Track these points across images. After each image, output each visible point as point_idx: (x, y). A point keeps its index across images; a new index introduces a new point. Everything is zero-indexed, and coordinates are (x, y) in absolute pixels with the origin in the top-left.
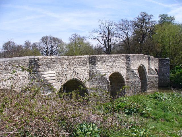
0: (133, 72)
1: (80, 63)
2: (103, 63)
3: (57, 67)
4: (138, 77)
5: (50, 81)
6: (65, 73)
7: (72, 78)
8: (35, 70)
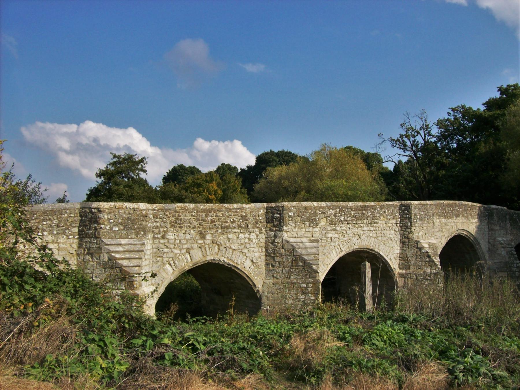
0: (420, 249)
1: (234, 222)
2: (307, 223)
3: (161, 230)
4: (435, 264)
5: (125, 263)
6: (185, 246)
7: (209, 258)
8: (92, 234)
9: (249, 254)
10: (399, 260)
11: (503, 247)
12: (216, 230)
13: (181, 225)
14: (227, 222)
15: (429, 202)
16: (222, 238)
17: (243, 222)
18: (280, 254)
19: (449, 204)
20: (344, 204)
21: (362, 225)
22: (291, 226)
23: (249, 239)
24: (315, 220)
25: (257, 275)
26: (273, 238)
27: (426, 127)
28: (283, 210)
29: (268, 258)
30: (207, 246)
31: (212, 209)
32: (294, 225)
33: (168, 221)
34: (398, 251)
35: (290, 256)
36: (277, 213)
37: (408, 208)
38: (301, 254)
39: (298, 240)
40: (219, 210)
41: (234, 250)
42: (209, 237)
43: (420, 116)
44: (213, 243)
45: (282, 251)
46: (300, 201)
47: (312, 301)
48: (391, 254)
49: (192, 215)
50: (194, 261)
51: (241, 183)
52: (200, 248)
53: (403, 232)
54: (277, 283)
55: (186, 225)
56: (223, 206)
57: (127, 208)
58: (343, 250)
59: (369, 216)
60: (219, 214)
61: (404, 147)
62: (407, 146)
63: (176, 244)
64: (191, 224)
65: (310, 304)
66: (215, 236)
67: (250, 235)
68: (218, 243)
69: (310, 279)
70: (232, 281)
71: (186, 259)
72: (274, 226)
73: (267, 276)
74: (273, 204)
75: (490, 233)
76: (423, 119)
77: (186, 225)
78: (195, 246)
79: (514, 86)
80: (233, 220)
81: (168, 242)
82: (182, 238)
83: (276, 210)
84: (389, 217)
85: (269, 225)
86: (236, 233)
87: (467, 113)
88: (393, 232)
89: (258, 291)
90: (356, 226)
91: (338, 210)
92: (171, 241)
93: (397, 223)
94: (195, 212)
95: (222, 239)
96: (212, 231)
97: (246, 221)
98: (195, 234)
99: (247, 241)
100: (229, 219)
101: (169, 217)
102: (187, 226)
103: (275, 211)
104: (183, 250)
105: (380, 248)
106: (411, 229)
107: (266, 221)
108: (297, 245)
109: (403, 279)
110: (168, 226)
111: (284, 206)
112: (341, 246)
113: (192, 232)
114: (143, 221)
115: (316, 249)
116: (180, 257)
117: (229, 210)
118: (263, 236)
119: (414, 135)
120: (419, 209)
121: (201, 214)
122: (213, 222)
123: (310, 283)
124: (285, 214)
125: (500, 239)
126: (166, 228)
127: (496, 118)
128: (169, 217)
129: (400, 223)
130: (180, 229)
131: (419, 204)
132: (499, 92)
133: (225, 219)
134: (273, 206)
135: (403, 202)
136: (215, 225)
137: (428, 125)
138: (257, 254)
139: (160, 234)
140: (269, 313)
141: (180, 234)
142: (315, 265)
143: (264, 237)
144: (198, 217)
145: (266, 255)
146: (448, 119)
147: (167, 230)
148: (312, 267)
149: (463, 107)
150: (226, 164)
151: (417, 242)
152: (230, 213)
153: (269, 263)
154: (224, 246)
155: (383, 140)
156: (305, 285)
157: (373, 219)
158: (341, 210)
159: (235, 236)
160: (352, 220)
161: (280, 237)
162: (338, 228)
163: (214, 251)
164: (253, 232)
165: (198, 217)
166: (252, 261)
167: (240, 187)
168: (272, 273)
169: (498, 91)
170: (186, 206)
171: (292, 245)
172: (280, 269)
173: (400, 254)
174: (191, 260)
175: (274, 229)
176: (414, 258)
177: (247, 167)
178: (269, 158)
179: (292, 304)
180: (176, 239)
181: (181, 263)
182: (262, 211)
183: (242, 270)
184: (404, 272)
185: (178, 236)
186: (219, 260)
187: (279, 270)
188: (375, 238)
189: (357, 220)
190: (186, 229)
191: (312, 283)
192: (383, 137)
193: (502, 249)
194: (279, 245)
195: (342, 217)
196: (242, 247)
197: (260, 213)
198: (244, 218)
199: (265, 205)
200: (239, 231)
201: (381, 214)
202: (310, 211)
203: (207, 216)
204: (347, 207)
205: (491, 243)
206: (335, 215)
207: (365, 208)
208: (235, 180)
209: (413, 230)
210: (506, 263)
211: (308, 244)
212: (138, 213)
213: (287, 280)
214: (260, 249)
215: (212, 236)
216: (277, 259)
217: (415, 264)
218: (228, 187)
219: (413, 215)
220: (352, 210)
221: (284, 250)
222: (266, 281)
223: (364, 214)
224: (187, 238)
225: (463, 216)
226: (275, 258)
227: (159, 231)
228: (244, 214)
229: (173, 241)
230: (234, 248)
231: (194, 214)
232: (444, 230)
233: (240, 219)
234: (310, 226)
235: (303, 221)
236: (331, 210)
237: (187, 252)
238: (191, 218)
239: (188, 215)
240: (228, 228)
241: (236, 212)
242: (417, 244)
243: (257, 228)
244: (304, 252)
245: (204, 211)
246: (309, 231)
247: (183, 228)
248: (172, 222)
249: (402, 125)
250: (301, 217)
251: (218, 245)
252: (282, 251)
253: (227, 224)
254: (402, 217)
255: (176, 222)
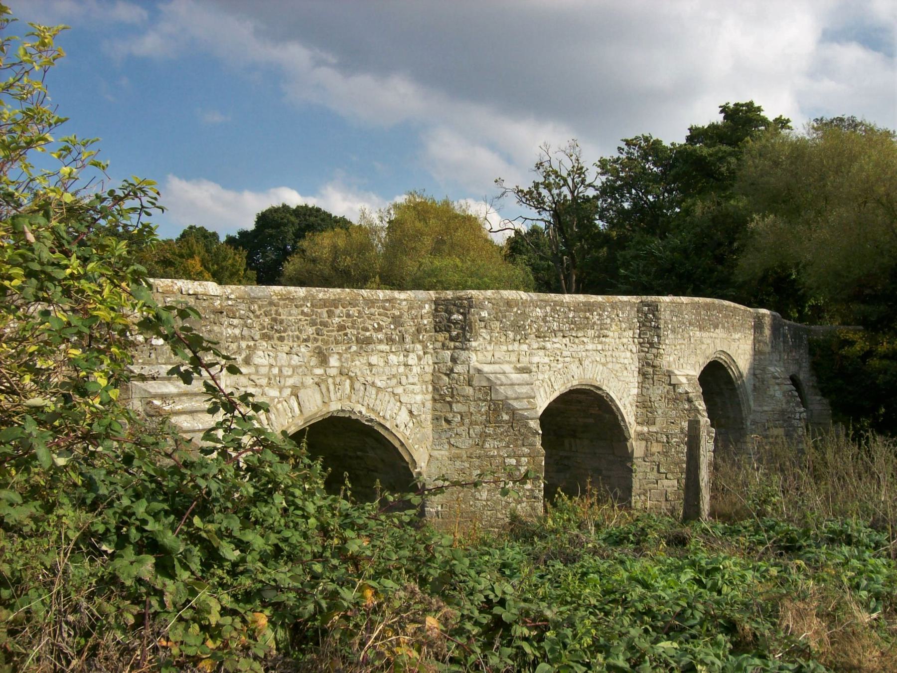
1: (380, 329)
2: (511, 335)
3: (244, 344)
6: (290, 382)
7: (334, 407)
9: (406, 398)
10: (637, 406)
11: (778, 384)
12: (348, 346)
13: (283, 334)
14: (367, 330)
15: (684, 299)
16: (357, 363)
17: (395, 329)
18: (463, 396)
19: (706, 304)
20: (557, 299)
21: (585, 340)
22: (484, 338)
23: (406, 365)
24: (524, 329)
25: (420, 441)
26: (450, 364)
27: (580, 171)
28: (471, 307)
29: (438, 405)
30: (330, 381)
31: (340, 300)
32: (488, 337)
33: (256, 325)
34: (635, 391)
35: (485, 401)
36: (458, 312)
37: (654, 308)
38: (507, 398)
39: (496, 368)
40: (352, 303)
41: (379, 389)
42: (334, 361)
43: (568, 151)
44: (341, 374)
45: (469, 391)
46: (498, 289)
47: (528, 494)
48: (625, 395)
49: (303, 313)
50: (307, 413)
51: (245, 260)
52: (318, 384)
53: (643, 354)
54: (458, 457)
55: (291, 333)
56: (359, 295)
57: (181, 293)
58: (556, 388)
59: (595, 323)
60: (353, 311)
61: (539, 204)
62: (544, 203)
63: (271, 376)
64: (300, 331)
65: (524, 499)
66: (347, 359)
67: (407, 356)
68: (350, 373)
69: (524, 449)
70: (359, 453)
71: (292, 410)
72: (452, 339)
73: (437, 442)
74: (448, 292)
75: (757, 357)
76: (573, 158)
77: (291, 333)
78: (309, 381)
79: (747, 105)
80: (378, 324)
81: (257, 371)
82: (284, 363)
83: (455, 305)
84: (624, 326)
85: (441, 337)
86: (382, 352)
87: (653, 149)
88: (628, 354)
89: (420, 474)
90: (577, 340)
91: (548, 309)
92: (264, 370)
93: (634, 338)
94: (309, 305)
95: (358, 366)
96: (341, 348)
97: (401, 328)
98: (310, 354)
99: (402, 369)
100: (370, 322)
101: (258, 317)
102: (293, 336)
103: (454, 309)
104: (285, 390)
105: (610, 385)
106: (658, 349)
107: (435, 328)
108: (497, 378)
109: (644, 443)
110: (257, 337)
111: (471, 298)
112: (553, 379)
113: (303, 349)
114: (215, 323)
115: (528, 387)
116: (279, 406)
117: (370, 303)
118: (429, 359)
119: (559, 184)
120: (671, 311)
121: (319, 310)
122: (341, 328)
123: (524, 456)
124: (473, 315)
125: (772, 369)
126: (253, 339)
127: (721, 159)
128: (258, 317)
129: (640, 337)
130: (279, 343)
131: (672, 302)
132: (723, 115)
133: (364, 322)
134: (449, 297)
135: (644, 298)
136: (346, 335)
137: (582, 168)
138: (419, 398)
139: (240, 354)
140: (440, 520)
141: (279, 354)
142: (532, 419)
143: (431, 362)
144: (314, 317)
145: (434, 400)
146: (618, 159)
147: (255, 345)
148: (527, 423)
149: (646, 139)
150: (198, 227)
151: (669, 374)
152: (372, 310)
153: (441, 417)
154: (362, 380)
155: (504, 190)
156: (513, 461)
157: (601, 329)
158: (553, 310)
159: (382, 360)
160: (570, 330)
161: (464, 362)
162: (548, 345)
163: (343, 391)
164: (413, 351)
165: (314, 317)
166: (411, 412)
167: (245, 267)
168: (448, 436)
169: (721, 112)
170: (290, 293)
171: (488, 379)
172: (462, 428)
173: (638, 395)
174: (301, 411)
175: (452, 344)
176: (663, 404)
177: (239, 233)
178: (282, 219)
179: (487, 500)
180: (271, 366)
181: (281, 420)
182: (427, 306)
183: (394, 431)
184: (645, 429)
185: (276, 358)
186: (352, 412)
187: (460, 430)
188: (604, 365)
189: (579, 329)
190: (291, 344)
191: (529, 455)
192: (504, 185)
193: (777, 387)
194: (462, 378)
195: (555, 324)
196: (394, 381)
197: (425, 311)
198: (397, 321)
199: (432, 294)
200: (388, 347)
201: (612, 320)
202: (515, 309)
203: (330, 314)
204: (562, 304)
205: (759, 376)
206: (544, 320)
207: (589, 308)
208: (235, 254)
209: (662, 351)
210: (783, 412)
211: (516, 377)
212: (205, 304)
213: (478, 452)
214: (424, 387)
215: (340, 359)
216: (456, 407)
217: (665, 414)
218: (222, 268)
219: (662, 322)
220: (570, 310)
221: (471, 389)
222: (435, 453)
223: (588, 318)
224: (293, 362)
225: (723, 327)
226: (454, 406)
227: (239, 347)
228: (397, 313)
229: (267, 368)
230: (379, 384)
231: (306, 310)
232: (698, 352)
233: (390, 323)
234: (514, 340)
235: (504, 329)
236: (538, 310)
237: (292, 394)
238: (300, 320)
239: (295, 311)
240: (368, 341)
241: (384, 308)
242: (670, 376)
243: (420, 342)
244: (510, 393)
245: (325, 303)
246: (513, 351)
247: (286, 342)
248: (264, 328)
249: (539, 166)
250: (501, 322)
251: (350, 378)
252: (469, 391)
253: (368, 334)
254: (644, 325)
255: (272, 328)
